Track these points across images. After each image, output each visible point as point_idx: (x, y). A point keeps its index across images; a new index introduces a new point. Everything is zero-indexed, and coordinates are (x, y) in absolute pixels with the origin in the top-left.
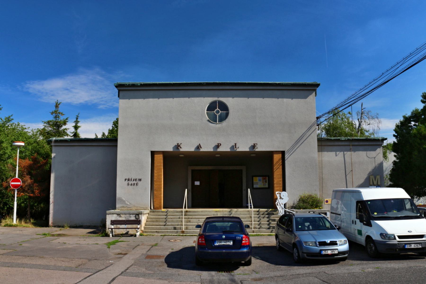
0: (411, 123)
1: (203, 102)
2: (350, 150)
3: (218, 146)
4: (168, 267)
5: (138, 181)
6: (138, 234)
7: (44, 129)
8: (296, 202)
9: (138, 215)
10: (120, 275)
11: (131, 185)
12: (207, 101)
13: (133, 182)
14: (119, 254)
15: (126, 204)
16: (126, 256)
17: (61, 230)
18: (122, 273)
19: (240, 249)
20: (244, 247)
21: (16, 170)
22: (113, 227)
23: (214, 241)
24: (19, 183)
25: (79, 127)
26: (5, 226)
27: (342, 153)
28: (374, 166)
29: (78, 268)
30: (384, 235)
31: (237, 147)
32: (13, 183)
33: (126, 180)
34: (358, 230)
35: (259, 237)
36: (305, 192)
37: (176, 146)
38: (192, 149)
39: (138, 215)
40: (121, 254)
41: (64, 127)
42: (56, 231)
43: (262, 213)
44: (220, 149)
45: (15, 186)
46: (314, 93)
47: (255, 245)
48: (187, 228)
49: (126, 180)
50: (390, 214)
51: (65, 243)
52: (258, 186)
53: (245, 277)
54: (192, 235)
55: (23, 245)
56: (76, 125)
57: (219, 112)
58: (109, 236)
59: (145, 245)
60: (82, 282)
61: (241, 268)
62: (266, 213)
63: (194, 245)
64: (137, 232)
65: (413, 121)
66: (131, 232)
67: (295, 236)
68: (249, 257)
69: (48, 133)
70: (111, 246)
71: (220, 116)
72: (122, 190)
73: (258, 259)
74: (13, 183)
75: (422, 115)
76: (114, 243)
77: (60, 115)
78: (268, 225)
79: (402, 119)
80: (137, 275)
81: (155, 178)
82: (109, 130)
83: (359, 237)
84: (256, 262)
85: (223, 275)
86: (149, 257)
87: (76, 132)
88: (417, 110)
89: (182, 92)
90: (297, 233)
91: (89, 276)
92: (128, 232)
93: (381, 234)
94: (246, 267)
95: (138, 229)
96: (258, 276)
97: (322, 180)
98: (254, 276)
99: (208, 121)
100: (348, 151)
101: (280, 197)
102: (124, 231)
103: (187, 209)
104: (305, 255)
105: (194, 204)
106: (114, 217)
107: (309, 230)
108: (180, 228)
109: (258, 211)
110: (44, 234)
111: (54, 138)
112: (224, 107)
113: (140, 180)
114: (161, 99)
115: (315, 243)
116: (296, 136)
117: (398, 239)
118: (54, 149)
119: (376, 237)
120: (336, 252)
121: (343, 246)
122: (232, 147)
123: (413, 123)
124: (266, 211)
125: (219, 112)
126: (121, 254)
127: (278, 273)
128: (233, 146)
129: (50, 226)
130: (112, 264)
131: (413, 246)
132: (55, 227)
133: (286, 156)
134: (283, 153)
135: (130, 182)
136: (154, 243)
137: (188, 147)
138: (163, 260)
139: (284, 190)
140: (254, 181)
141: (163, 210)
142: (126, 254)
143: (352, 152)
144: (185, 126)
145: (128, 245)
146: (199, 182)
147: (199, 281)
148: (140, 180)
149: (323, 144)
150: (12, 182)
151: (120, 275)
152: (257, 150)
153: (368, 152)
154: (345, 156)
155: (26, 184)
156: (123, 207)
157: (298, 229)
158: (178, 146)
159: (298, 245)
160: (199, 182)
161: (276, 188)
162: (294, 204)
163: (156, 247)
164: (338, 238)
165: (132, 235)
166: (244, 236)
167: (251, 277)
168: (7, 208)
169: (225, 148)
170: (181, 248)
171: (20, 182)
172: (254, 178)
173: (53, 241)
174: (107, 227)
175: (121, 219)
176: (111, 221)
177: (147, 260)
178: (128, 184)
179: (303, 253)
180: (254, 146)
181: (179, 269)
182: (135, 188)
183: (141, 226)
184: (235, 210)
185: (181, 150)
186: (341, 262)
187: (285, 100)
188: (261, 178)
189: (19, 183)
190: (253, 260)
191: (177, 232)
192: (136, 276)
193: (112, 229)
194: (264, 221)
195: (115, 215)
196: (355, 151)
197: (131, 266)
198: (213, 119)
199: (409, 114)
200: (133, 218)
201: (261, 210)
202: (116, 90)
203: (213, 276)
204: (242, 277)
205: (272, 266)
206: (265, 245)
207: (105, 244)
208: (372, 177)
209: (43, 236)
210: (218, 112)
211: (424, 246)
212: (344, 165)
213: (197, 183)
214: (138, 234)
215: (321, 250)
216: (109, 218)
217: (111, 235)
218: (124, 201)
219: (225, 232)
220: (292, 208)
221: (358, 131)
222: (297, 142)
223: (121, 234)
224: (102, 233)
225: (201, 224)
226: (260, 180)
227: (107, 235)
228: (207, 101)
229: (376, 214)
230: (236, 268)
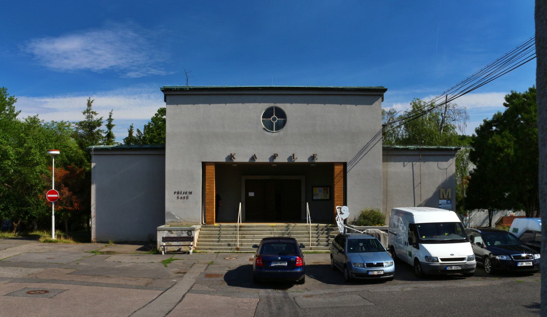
0: (492, 129)
1: (257, 110)
2: (419, 161)
3: (274, 157)
4: (228, 285)
5: (188, 194)
6: (191, 251)
7: (76, 132)
8: (357, 218)
9: (191, 231)
10: (187, 292)
11: (181, 198)
12: (263, 107)
13: (183, 196)
14: (178, 273)
15: (175, 219)
16: (186, 275)
17: (106, 246)
18: (189, 291)
19: (294, 269)
20: (298, 267)
21: (52, 181)
22: (164, 244)
23: (270, 262)
24: (56, 196)
25: (113, 126)
26: (44, 242)
27: (411, 163)
28: (445, 178)
29: (147, 286)
30: (429, 258)
31: (295, 158)
32: (49, 196)
33: (175, 193)
34: (409, 252)
35: (316, 254)
36: (367, 207)
37: (229, 156)
38: (247, 160)
39: (191, 231)
40: (180, 273)
41: (97, 128)
42: (103, 248)
43: (321, 228)
44: (277, 160)
45: (51, 199)
46: (381, 99)
47: (309, 264)
48: (241, 245)
49: (175, 193)
50: (438, 238)
51: (120, 262)
52: (319, 198)
53: (298, 294)
54: (247, 253)
55: (80, 264)
56: (109, 123)
57: (275, 120)
58: (161, 253)
59: (201, 263)
60: (158, 298)
61: (295, 286)
62: (326, 228)
63: (251, 263)
64: (190, 249)
65: (495, 126)
66: (184, 249)
67: (346, 257)
68: (303, 276)
69: (81, 136)
70: (168, 265)
71: (276, 124)
72: (171, 204)
73: (312, 278)
74: (49, 196)
75: (504, 120)
76: (169, 261)
77: (93, 115)
78: (327, 242)
79: (482, 123)
80: (203, 292)
81: (207, 191)
82: (145, 126)
83: (409, 258)
84: (309, 280)
85: (279, 293)
86: (208, 276)
87: (110, 132)
88: (499, 114)
89: (235, 97)
90: (349, 255)
91: (162, 293)
92: (180, 249)
93: (426, 257)
94: (299, 286)
95: (191, 246)
96: (309, 293)
97: (386, 193)
98: (307, 293)
99: (264, 129)
100: (417, 161)
101: (341, 211)
102: (176, 249)
103: (241, 224)
104: (354, 275)
105: (248, 218)
106: (165, 234)
107: (362, 251)
108: (235, 245)
109: (317, 227)
110: (93, 252)
111: (94, 147)
112: (281, 114)
113: (191, 193)
114: (212, 105)
115: (363, 264)
116: (360, 147)
117: (440, 261)
118: (93, 158)
119: (422, 259)
120: (382, 273)
121: (389, 267)
122: (290, 158)
123: (494, 128)
124: (326, 227)
125: (275, 120)
126: (180, 273)
127: (327, 291)
128: (291, 157)
129: (93, 242)
130: (176, 283)
131: (454, 268)
132: (97, 242)
133: (348, 168)
134: (345, 165)
135: (180, 196)
136: (210, 261)
137: (242, 158)
138: (223, 279)
139: (345, 204)
140: (314, 192)
141: (216, 225)
142: (185, 273)
143: (422, 163)
144: (240, 135)
145: (184, 263)
146: (253, 193)
147: (258, 296)
148: (191, 193)
149: (390, 154)
150: (49, 194)
151: (187, 292)
152: (316, 161)
153: (440, 163)
154: (414, 167)
155: (64, 196)
156: (173, 222)
157: (350, 251)
158: (231, 157)
159: (348, 265)
160: (253, 193)
161: (336, 203)
162: (355, 219)
163: (213, 266)
164: (385, 259)
165: (184, 253)
166: (298, 257)
167: (302, 295)
168: (28, 217)
169: (282, 159)
170: (238, 266)
171: (57, 194)
172: (314, 188)
173: (107, 260)
174: (158, 243)
175: (172, 235)
176: (163, 238)
177: (207, 279)
178: (178, 198)
179: (352, 273)
180: (313, 157)
181: (239, 288)
182: (185, 203)
183: (194, 243)
184: (293, 224)
185: (235, 161)
186: (388, 282)
187: (348, 106)
188: (322, 189)
189: (56, 196)
190: (307, 278)
191: (231, 249)
192: (203, 293)
193: (164, 246)
194: (323, 238)
195: (166, 232)
196: (425, 161)
197: (194, 284)
198: (269, 127)
199: (490, 118)
200: (185, 235)
201: (320, 225)
202: (162, 95)
203: (269, 293)
204: (295, 294)
205: (324, 285)
206: (321, 264)
207: (160, 262)
208: (442, 190)
209: (92, 254)
210: (275, 119)
211: (463, 268)
212: (412, 177)
213: (251, 194)
214: (191, 251)
215: (368, 271)
216: (160, 236)
217: (163, 252)
218: (174, 216)
219: (280, 255)
220: (352, 224)
221: (441, 129)
222: (360, 153)
223: (173, 251)
224: (153, 251)
225: (258, 244)
226: (320, 191)
227: (159, 253)
228: (263, 107)
229: (424, 237)
230: (290, 286)
